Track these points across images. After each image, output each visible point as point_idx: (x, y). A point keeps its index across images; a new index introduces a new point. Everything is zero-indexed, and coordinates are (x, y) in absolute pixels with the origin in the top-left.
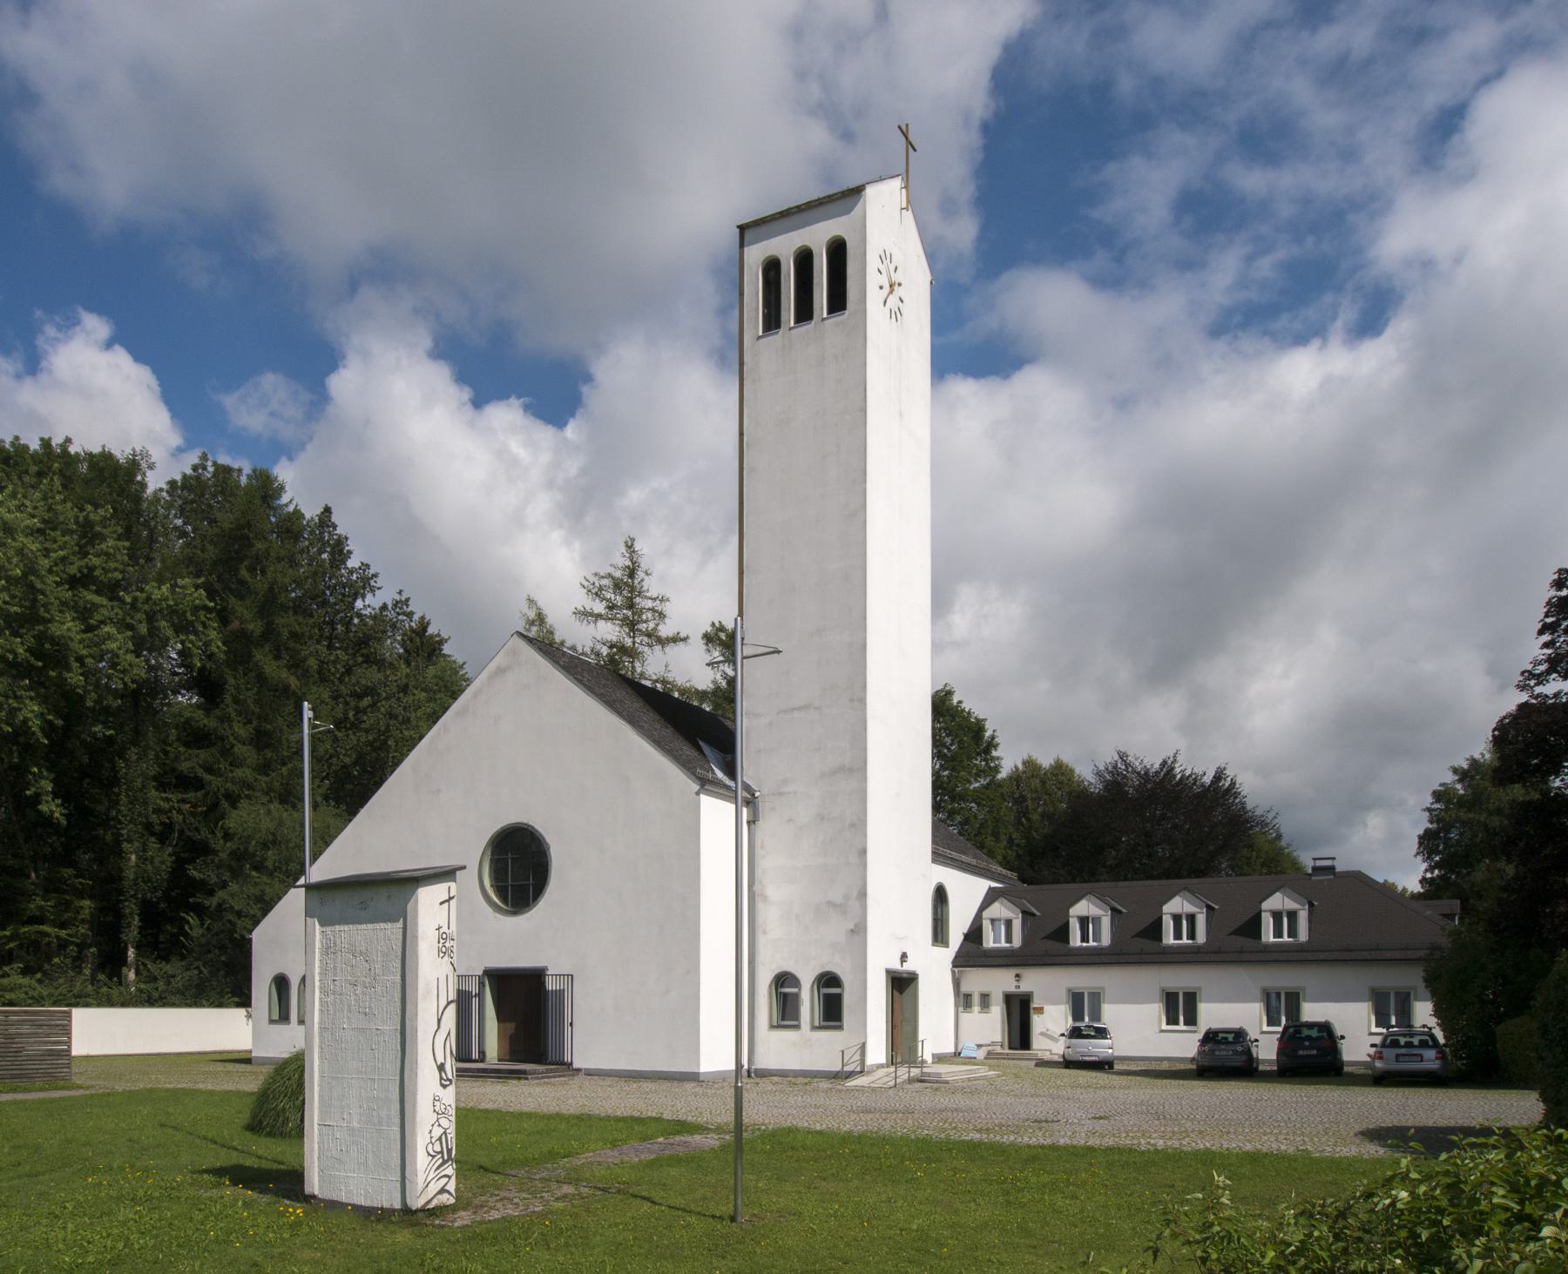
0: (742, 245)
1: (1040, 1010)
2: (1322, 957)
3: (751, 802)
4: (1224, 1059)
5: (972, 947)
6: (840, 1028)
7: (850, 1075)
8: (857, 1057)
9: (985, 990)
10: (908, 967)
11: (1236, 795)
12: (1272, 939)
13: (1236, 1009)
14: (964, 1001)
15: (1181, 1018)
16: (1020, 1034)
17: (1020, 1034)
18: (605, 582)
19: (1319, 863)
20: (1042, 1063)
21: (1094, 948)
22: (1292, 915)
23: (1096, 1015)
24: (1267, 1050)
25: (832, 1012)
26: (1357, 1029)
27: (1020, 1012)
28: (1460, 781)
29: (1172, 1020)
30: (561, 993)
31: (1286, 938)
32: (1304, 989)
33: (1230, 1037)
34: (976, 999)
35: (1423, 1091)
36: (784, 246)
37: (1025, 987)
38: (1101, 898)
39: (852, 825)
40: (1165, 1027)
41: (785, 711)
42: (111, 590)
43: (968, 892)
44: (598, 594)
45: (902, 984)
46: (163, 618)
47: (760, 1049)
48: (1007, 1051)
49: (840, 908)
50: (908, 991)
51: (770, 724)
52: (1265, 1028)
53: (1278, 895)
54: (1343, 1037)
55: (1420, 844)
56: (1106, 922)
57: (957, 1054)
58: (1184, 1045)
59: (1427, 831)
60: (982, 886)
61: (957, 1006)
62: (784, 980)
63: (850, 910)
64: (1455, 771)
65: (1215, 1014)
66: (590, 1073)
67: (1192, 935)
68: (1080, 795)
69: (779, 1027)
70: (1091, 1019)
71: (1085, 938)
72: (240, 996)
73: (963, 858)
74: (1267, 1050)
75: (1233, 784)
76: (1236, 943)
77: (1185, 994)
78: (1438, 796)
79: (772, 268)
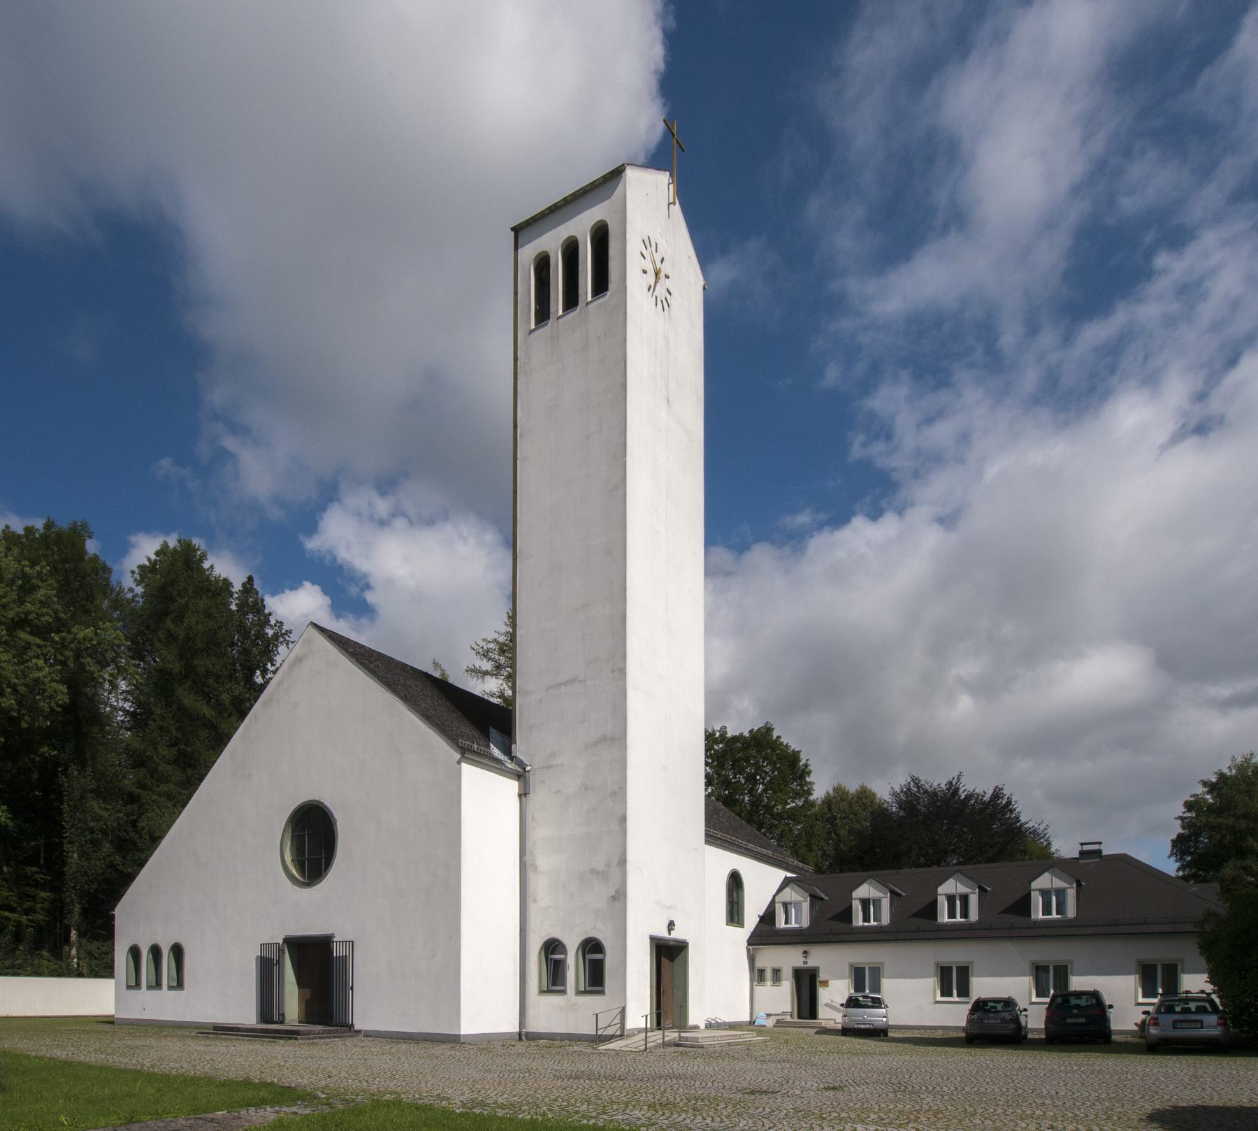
0: (516, 248)
1: (825, 983)
2: (1090, 931)
3: (521, 775)
4: (993, 1028)
5: (766, 927)
6: (602, 992)
7: (611, 1038)
8: (617, 1020)
9: (776, 965)
10: (677, 934)
11: (1012, 811)
12: (1041, 916)
13: (1008, 982)
14: (758, 975)
15: (955, 992)
16: (807, 1003)
17: (807, 1003)
18: (492, 646)
19: (1086, 848)
20: (824, 1031)
21: (874, 927)
22: (1061, 893)
23: (876, 987)
24: (1035, 1019)
25: (595, 978)
26: (1125, 1000)
27: (807, 986)
28: (1208, 793)
29: (946, 991)
30: (344, 959)
31: (1054, 915)
32: (1071, 962)
33: (999, 1007)
34: (769, 974)
35: (1206, 1058)
36: (551, 241)
37: (812, 963)
38: (883, 883)
39: (614, 794)
40: (939, 998)
41: (553, 687)
42: (42, 632)
43: (763, 881)
44: (485, 654)
45: (669, 954)
46: (90, 656)
47: (531, 1013)
48: (796, 1020)
49: (601, 875)
50: (679, 960)
51: (540, 700)
52: (1034, 999)
53: (1046, 876)
54: (1111, 1007)
55: (1173, 846)
56: (886, 903)
57: (752, 1023)
58: (955, 1015)
59: (1179, 836)
60: (777, 875)
61: (752, 980)
62: (552, 947)
63: (610, 878)
64: (1205, 784)
65: (984, 986)
66: (368, 1034)
67: (965, 914)
68: (880, 814)
69: (549, 991)
70: (872, 991)
71: (866, 919)
72: (105, 970)
73: (750, 846)
74: (1035, 1019)
75: (1009, 802)
76: (1008, 921)
77: (958, 968)
78: (1189, 806)
79: (543, 264)
